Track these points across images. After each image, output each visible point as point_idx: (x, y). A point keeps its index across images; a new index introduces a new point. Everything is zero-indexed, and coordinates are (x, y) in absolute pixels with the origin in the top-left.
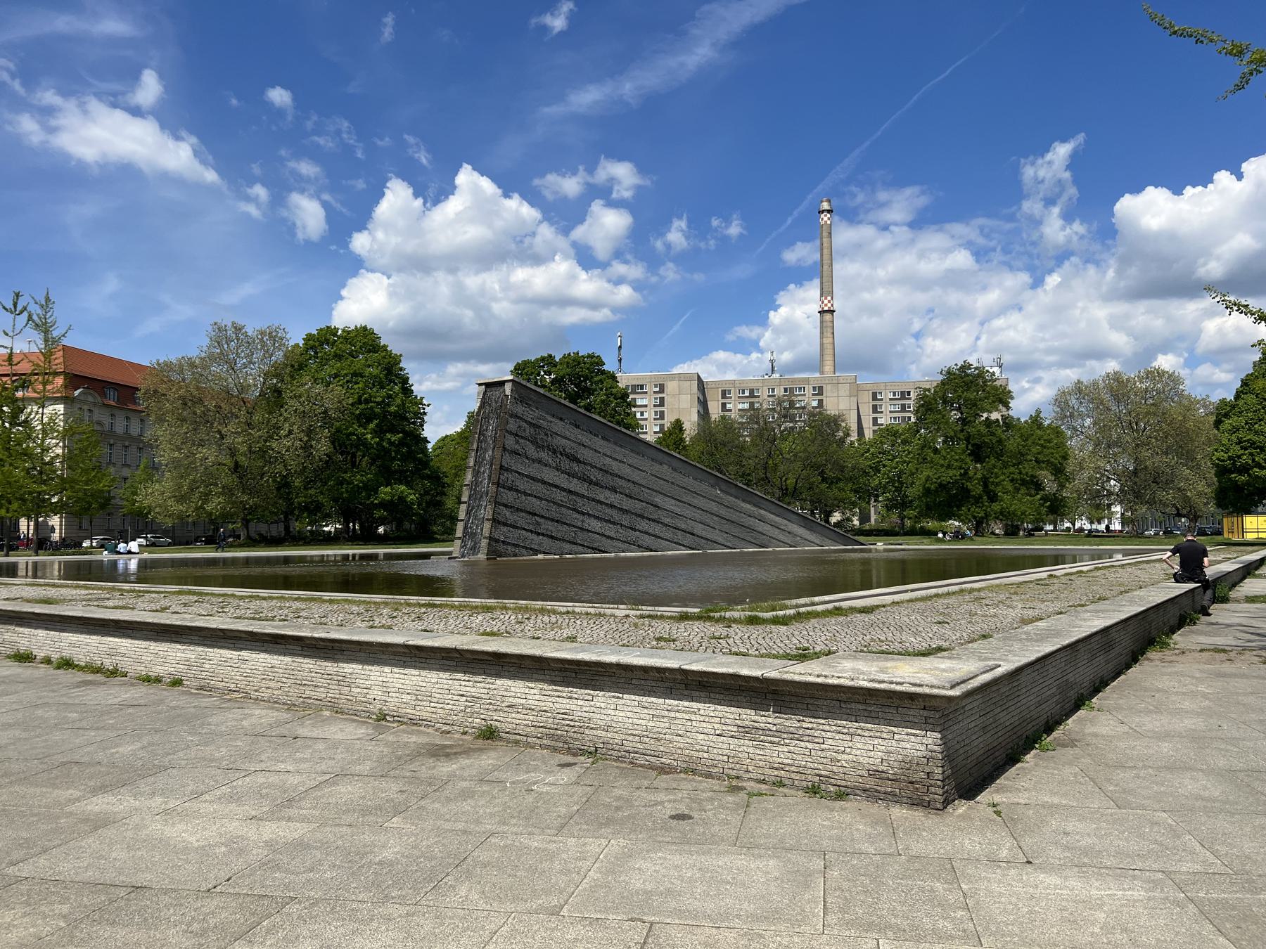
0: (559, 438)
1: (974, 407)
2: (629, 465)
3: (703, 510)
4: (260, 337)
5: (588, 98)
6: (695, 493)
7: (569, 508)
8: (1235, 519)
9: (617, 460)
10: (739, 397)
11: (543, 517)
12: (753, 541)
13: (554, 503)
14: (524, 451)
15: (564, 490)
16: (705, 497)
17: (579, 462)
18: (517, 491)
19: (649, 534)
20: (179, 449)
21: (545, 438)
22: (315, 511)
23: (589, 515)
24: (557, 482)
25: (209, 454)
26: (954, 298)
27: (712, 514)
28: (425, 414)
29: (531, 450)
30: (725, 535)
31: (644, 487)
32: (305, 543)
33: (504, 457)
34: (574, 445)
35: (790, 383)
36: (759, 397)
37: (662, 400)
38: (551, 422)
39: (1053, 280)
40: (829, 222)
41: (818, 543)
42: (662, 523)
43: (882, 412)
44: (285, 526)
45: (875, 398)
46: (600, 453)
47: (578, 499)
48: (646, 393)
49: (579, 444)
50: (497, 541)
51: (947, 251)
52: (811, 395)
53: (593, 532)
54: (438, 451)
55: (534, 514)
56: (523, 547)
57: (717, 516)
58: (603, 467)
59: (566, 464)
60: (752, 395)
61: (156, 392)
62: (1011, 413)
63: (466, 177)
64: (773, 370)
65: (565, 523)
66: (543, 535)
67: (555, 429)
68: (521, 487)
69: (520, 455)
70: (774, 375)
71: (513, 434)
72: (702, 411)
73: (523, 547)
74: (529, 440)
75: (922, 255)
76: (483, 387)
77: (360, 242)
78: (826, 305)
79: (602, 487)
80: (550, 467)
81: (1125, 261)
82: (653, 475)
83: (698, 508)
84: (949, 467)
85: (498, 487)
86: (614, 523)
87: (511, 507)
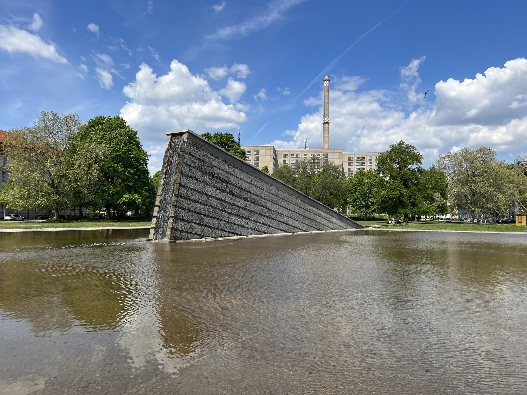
0: (215, 169)
1: (404, 163)
2: (255, 186)
3: (292, 211)
4: (65, 119)
5: (226, 32)
6: (288, 201)
7: (221, 210)
8: (523, 217)
9: (248, 182)
10: (291, 158)
11: (205, 215)
12: (316, 227)
13: (212, 207)
14: (194, 176)
15: (218, 199)
16: (293, 204)
17: (227, 183)
18: (190, 199)
19: (265, 224)
20: (21, 173)
21: (208, 168)
22: (94, 205)
23: (232, 214)
24: (214, 194)
25: (37, 176)
26: (373, 122)
27: (296, 213)
28: (148, 160)
29: (199, 175)
30: (303, 224)
31: (262, 198)
32: (89, 220)
33: (182, 179)
34: (225, 173)
36: (300, 157)
37: (258, 158)
38: (211, 159)
39: (413, 115)
40: (328, 85)
41: (345, 227)
42: (271, 218)
43: (352, 166)
44: (80, 211)
45: (349, 159)
46: (239, 178)
47: (226, 205)
48: (251, 154)
49: (227, 172)
50: (176, 230)
51: (371, 102)
53: (234, 224)
54: (156, 178)
55: (201, 214)
56: (193, 233)
57: (299, 214)
58: (240, 187)
59: (219, 184)
60: (297, 157)
61: (11, 145)
62: (421, 166)
63: (175, 65)
64: (306, 146)
65: (218, 219)
66: (205, 226)
67: (214, 163)
68: (192, 197)
69: (192, 178)
70: (306, 148)
71: (188, 165)
72: (275, 163)
73: (193, 233)
74: (197, 169)
75: (360, 104)
76: (170, 136)
77: (127, 90)
78: (326, 120)
79: (240, 198)
80: (210, 185)
81: (439, 110)
82: (267, 191)
83: (290, 210)
84: (395, 189)
85: (178, 197)
86: (245, 218)
87: (186, 209)
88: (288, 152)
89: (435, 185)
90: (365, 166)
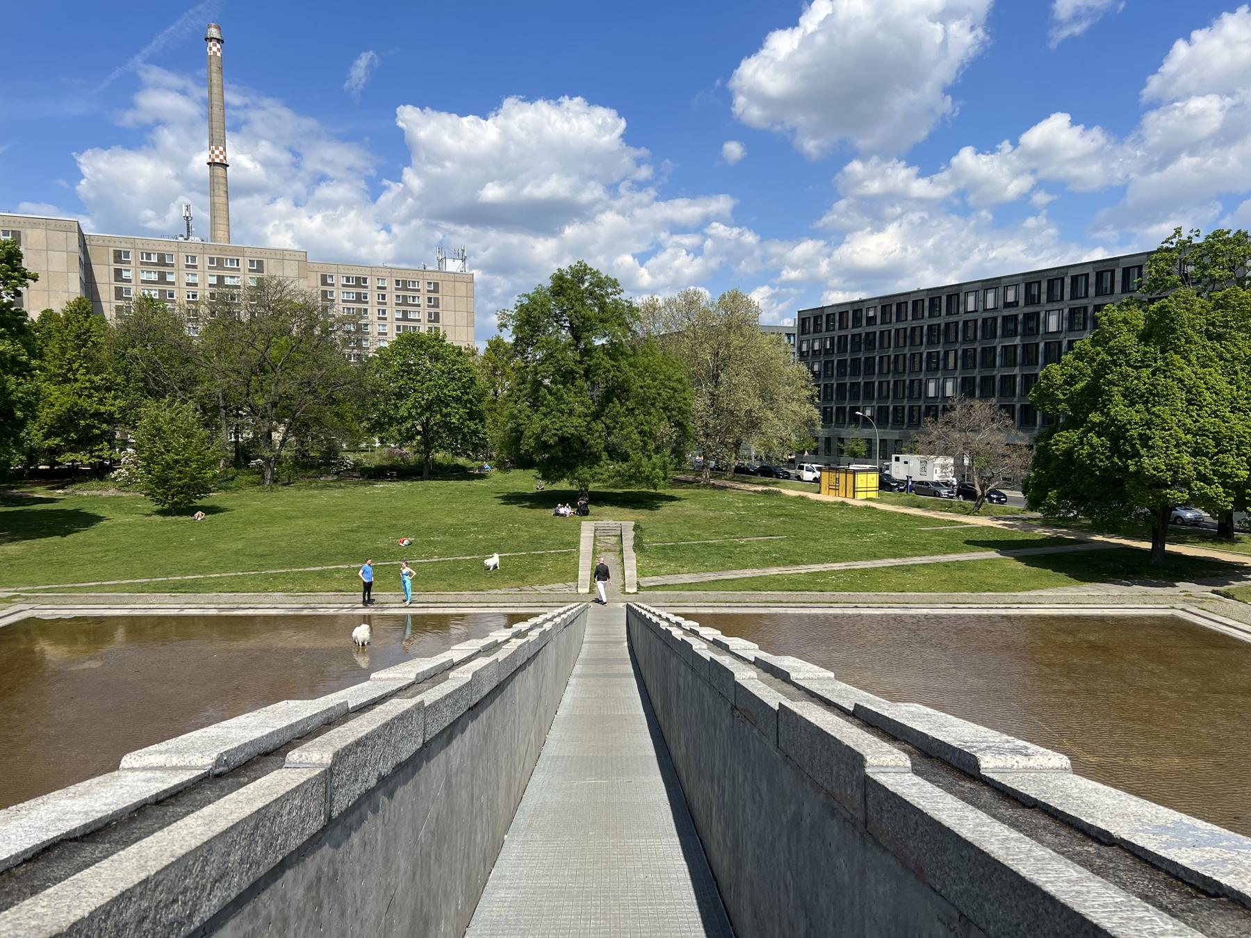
8: (842, 476)
33: (126, 766)
35: (218, 252)
40: (219, 54)
45: (324, 282)
52: (247, 272)
60: (162, 261)
64: (188, 231)
78: (217, 156)
88: (129, 246)
89: (669, 399)
90: (367, 303)
